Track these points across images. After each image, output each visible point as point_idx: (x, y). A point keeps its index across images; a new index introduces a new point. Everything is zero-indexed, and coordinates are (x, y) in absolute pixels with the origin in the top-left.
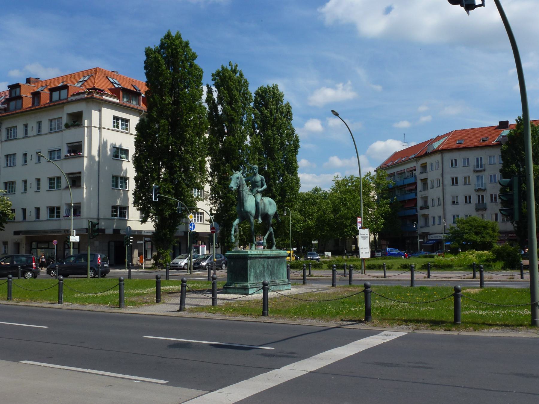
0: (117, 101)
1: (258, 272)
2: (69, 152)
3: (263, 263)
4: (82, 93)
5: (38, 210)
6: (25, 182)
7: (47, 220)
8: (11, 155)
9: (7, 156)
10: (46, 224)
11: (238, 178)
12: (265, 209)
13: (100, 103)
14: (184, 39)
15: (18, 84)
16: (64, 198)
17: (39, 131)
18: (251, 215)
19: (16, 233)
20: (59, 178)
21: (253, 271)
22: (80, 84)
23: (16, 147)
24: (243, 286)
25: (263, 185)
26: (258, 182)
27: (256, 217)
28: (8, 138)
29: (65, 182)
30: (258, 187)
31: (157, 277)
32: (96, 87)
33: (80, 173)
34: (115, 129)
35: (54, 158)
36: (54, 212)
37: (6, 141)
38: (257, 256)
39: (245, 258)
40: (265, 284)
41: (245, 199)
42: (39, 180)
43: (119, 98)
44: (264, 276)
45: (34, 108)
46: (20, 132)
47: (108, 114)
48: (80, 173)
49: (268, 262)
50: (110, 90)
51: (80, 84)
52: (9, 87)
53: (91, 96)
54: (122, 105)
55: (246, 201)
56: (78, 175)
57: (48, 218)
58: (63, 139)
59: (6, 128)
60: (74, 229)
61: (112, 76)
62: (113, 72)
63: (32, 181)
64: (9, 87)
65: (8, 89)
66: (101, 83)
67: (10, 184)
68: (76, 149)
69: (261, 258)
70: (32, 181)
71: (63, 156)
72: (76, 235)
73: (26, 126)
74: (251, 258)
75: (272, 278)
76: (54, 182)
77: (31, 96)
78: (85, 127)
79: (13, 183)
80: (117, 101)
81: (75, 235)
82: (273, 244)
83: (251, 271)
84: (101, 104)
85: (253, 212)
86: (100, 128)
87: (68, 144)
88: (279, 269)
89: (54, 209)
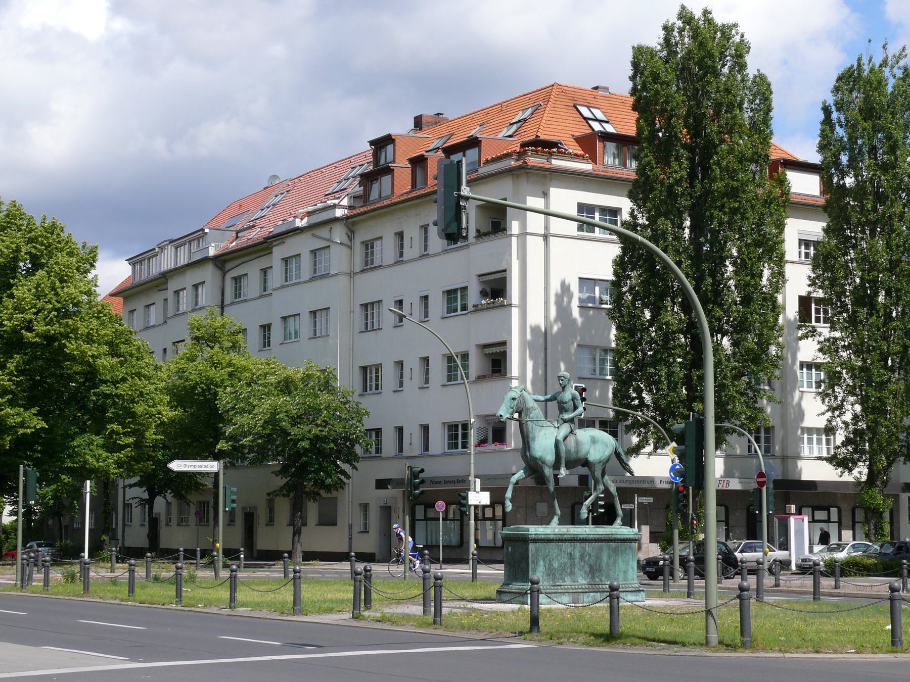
0: (587, 167)
1: (556, 565)
2: (484, 294)
3: (569, 551)
4: (508, 156)
5: (426, 429)
6: (400, 364)
7: (444, 454)
8: (373, 303)
9: (365, 306)
10: (440, 465)
11: (514, 399)
12: (577, 452)
13: (545, 176)
14: (720, 18)
15: (390, 135)
16: (471, 403)
17: (426, 249)
18: (543, 463)
19: (381, 484)
20: (465, 356)
21: (541, 563)
22: (515, 127)
23: (382, 286)
24: (522, 589)
25: (575, 408)
26: (566, 403)
27: (556, 466)
28: (366, 264)
29: (476, 365)
30: (566, 411)
31: (742, 589)
32: (543, 137)
33: (504, 343)
34: (585, 234)
35: (456, 310)
36: (457, 433)
37: (363, 271)
38: (552, 537)
39: (524, 540)
40: (613, 589)
41: (531, 436)
42: (426, 360)
43: (594, 160)
44: (572, 573)
45: (413, 194)
46: (386, 250)
47: (565, 199)
48: (504, 343)
49: (584, 549)
50: (579, 140)
51: (515, 127)
52: (372, 143)
53: (520, 162)
54: (598, 177)
55: (534, 439)
56: (501, 349)
57: (446, 450)
58: (464, 266)
59: (363, 243)
60: (476, 477)
61: (590, 100)
62: (596, 88)
63: (412, 364)
64: (372, 143)
65: (368, 147)
66: (558, 126)
67: (371, 370)
68: (496, 289)
69: (565, 540)
70: (412, 364)
71: (470, 304)
72: (483, 490)
73: (400, 235)
74: (535, 541)
75: (593, 577)
76: (454, 365)
77: (409, 166)
78: (511, 235)
79: (378, 368)
80: (587, 167)
81: (478, 488)
82: (555, 514)
83: (536, 564)
84: (550, 177)
85: (550, 458)
86: (546, 237)
87: (480, 276)
88: (615, 562)
89: (457, 426)
